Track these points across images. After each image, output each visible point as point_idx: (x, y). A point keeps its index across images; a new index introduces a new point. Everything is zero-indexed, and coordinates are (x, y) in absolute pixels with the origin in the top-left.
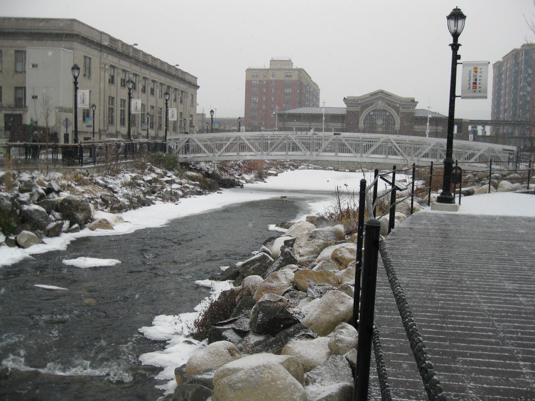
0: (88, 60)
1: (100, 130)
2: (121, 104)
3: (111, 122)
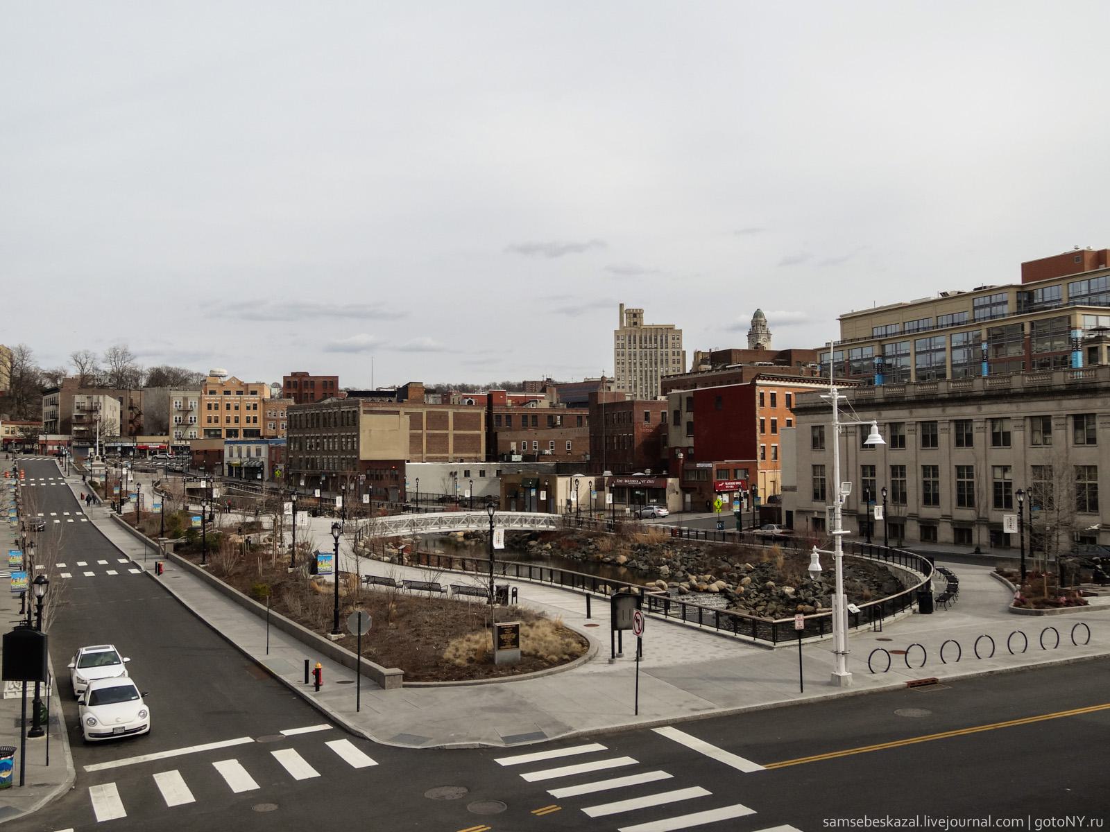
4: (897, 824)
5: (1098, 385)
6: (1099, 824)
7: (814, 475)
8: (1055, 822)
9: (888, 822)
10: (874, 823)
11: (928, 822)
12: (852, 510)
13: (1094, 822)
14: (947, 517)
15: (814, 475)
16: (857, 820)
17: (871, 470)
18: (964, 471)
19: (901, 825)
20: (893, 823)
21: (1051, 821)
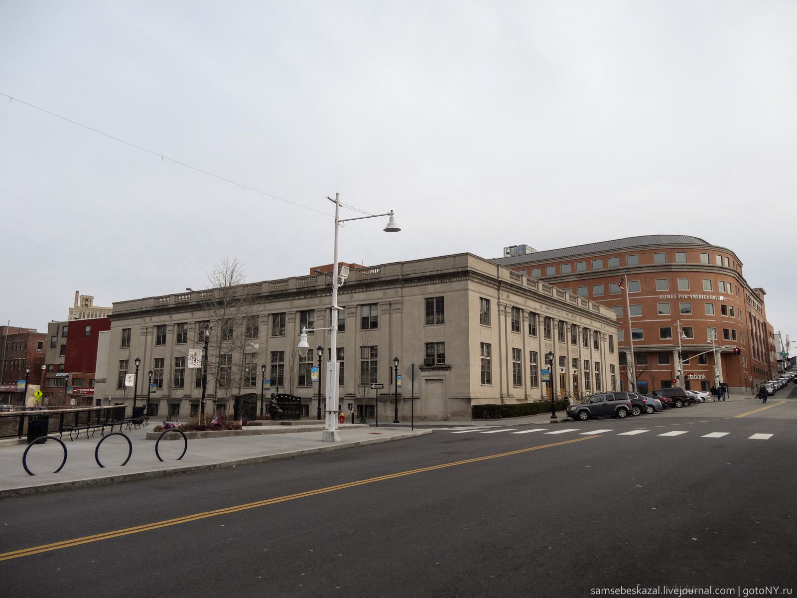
0: (485, 302)
1: (501, 395)
2: (531, 359)
3: (518, 380)
4: (644, 592)
5: (317, 288)
6: (789, 592)
7: (121, 369)
8: (758, 591)
9: (638, 591)
10: (627, 591)
11: (666, 590)
12: (144, 395)
13: (786, 591)
14: (187, 397)
15: (121, 369)
16: (615, 589)
17: (162, 362)
18: (278, 356)
19: (647, 593)
20: (641, 591)
21: (755, 590)
